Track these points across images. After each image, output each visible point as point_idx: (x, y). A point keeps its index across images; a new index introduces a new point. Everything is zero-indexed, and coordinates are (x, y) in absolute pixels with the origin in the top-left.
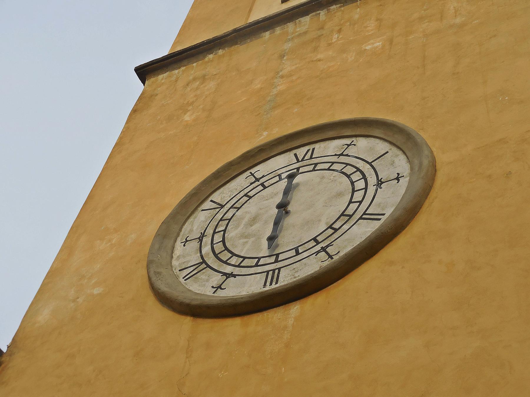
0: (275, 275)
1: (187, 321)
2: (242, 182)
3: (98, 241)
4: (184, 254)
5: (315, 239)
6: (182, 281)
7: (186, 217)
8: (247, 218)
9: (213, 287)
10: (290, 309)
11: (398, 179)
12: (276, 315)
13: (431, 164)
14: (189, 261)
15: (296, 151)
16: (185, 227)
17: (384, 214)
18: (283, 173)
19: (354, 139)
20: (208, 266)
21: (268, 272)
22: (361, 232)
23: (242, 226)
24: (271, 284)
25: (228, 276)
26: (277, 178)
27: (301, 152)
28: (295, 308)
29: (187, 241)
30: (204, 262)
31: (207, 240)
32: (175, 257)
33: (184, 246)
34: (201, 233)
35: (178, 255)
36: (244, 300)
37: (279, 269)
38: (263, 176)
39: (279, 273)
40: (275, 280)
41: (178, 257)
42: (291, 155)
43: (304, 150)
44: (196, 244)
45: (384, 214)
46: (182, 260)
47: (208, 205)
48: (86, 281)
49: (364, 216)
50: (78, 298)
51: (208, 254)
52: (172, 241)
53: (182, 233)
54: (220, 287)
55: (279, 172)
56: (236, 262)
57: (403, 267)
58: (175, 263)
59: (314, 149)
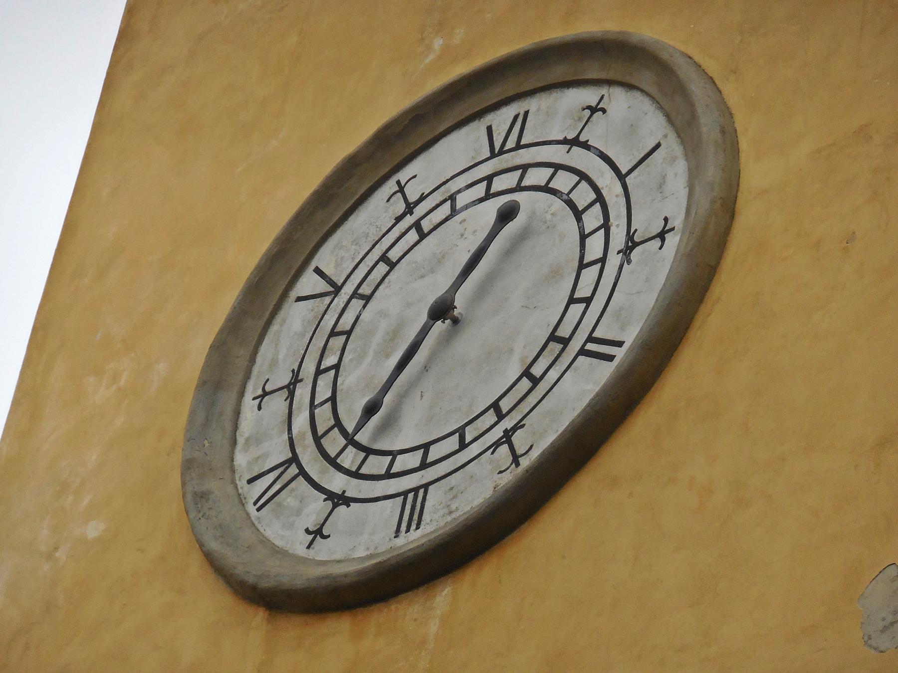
0: (413, 503)
1: (258, 617)
2: (379, 210)
3: (92, 379)
4: (261, 433)
5: (495, 406)
6: (252, 509)
7: (262, 323)
8: (384, 326)
9: (308, 531)
10: (435, 596)
11: (662, 236)
12: (411, 610)
13: (718, 205)
14: (265, 456)
15: (491, 119)
16: (263, 349)
17: (620, 344)
18: (459, 191)
19: (604, 91)
20: (303, 473)
21: (405, 494)
22: (581, 386)
23: (369, 359)
24: (408, 531)
25: (338, 500)
26: (446, 209)
27: (501, 119)
28: (445, 592)
29: (265, 394)
30: (294, 459)
31: (302, 392)
32: (241, 440)
33: (260, 408)
34: (293, 371)
35: (246, 435)
36: (348, 581)
37: (426, 486)
38: (422, 198)
39: (426, 493)
40: (416, 517)
41: (247, 440)
42: (474, 133)
43: (506, 115)
44: (277, 404)
45: (620, 344)
46: (255, 452)
47: (309, 283)
48: (70, 498)
49: (590, 347)
50: (56, 549)
51: (302, 435)
52: (233, 396)
53: (256, 370)
54: (318, 533)
55: (453, 186)
56: (353, 462)
57: (631, 495)
58: (241, 459)
59: (526, 113)
